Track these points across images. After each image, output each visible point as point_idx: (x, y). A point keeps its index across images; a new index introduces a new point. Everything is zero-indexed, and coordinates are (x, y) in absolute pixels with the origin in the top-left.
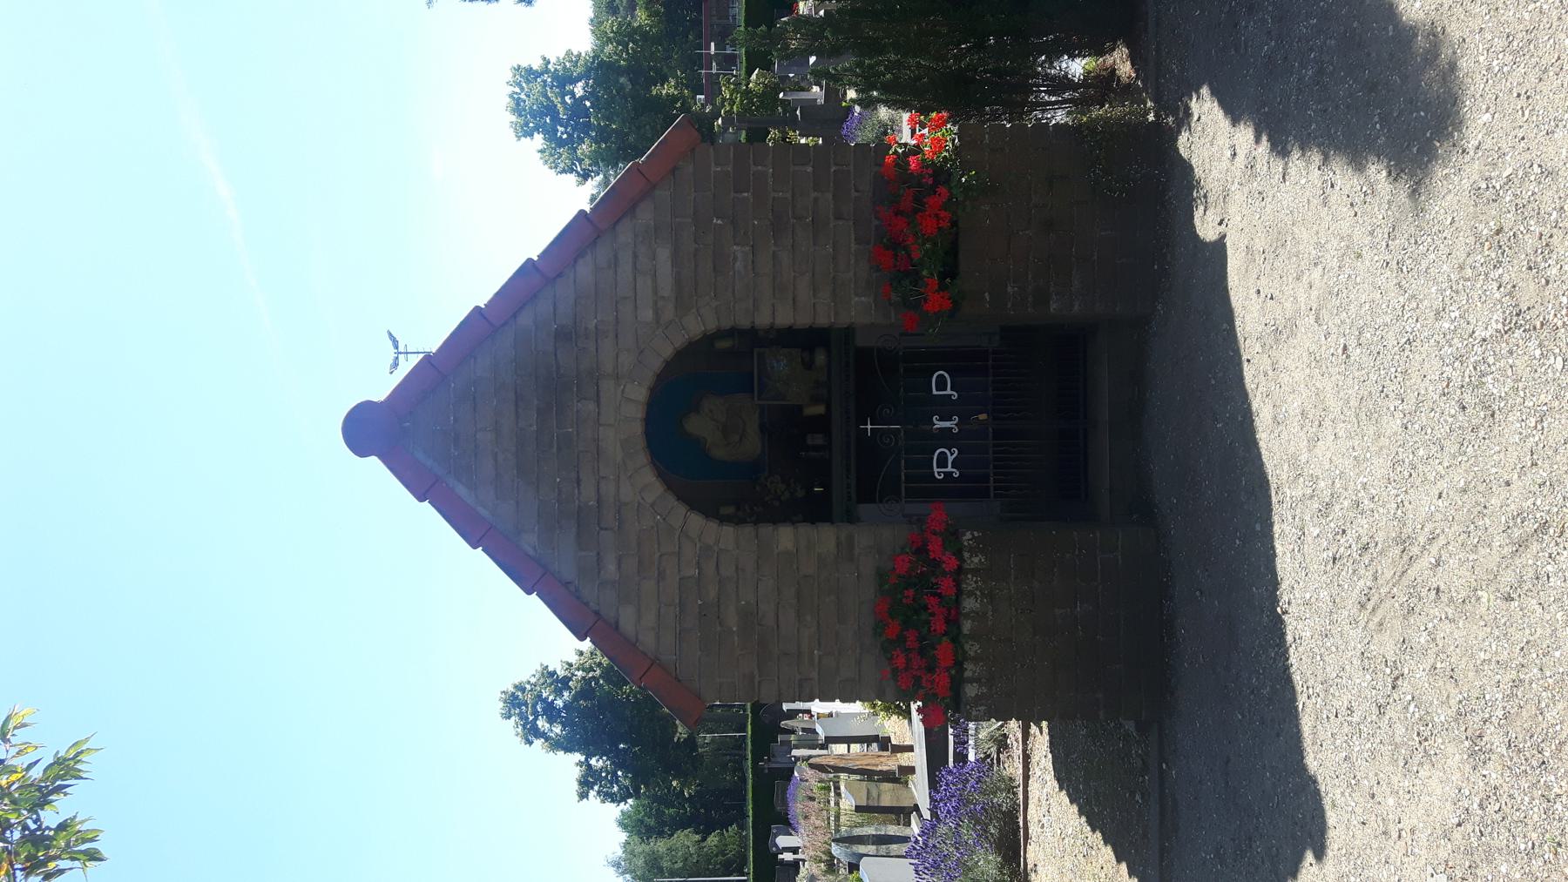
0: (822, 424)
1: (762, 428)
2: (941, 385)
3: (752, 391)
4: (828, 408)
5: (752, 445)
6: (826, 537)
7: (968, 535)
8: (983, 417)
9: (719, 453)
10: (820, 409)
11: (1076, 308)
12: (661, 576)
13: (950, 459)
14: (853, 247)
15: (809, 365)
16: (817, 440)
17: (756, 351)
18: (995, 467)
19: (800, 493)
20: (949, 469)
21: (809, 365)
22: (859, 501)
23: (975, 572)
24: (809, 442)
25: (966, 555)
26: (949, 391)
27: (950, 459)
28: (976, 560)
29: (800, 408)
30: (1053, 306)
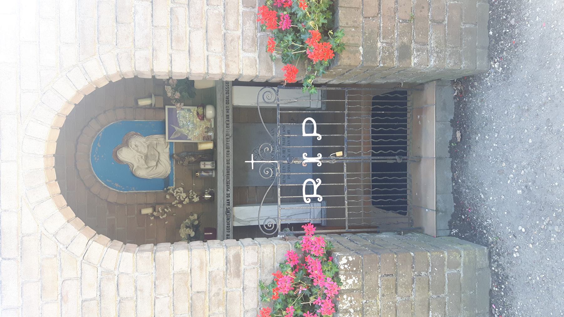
0: (211, 155)
1: (171, 157)
2: (310, 129)
3: (165, 133)
4: (215, 145)
5: (164, 167)
6: (214, 255)
7: (344, 260)
8: (339, 154)
9: (142, 173)
10: (209, 146)
11: (432, 63)
12: (63, 299)
13: (316, 187)
14: (241, 9)
15: (202, 117)
16: (208, 165)
17: (167, 107)
18: (349, 193)
19: (196, 199)
20: (315, 195)
21: (202, 117)
22: (235, 205)
23: (350, 291)
24: (202, 167)
25: (342, 278)
26: (315, 134)
27: (316, 187)
28: (350, 281)
29: (196, 144)
30: (414, 61)
